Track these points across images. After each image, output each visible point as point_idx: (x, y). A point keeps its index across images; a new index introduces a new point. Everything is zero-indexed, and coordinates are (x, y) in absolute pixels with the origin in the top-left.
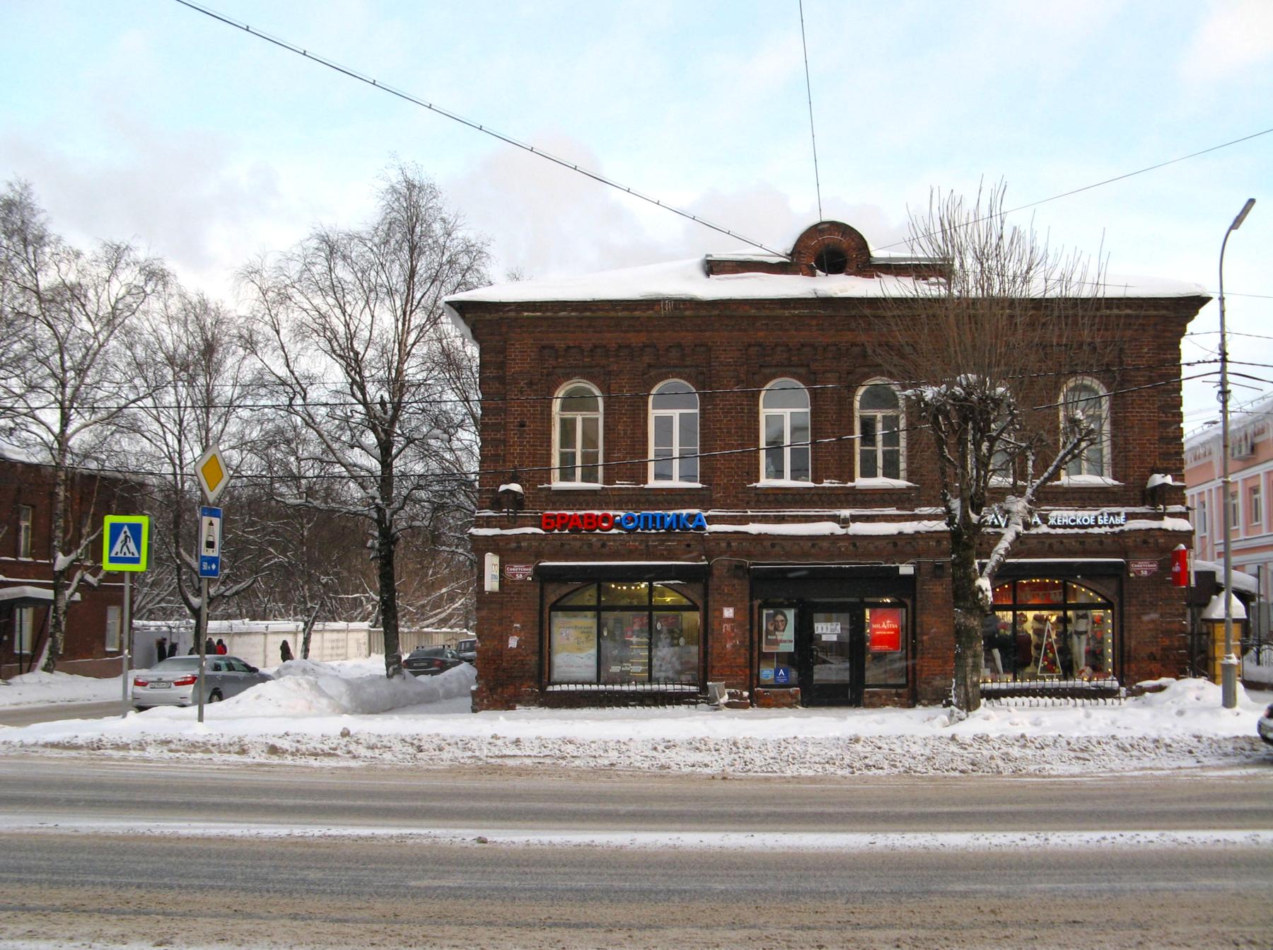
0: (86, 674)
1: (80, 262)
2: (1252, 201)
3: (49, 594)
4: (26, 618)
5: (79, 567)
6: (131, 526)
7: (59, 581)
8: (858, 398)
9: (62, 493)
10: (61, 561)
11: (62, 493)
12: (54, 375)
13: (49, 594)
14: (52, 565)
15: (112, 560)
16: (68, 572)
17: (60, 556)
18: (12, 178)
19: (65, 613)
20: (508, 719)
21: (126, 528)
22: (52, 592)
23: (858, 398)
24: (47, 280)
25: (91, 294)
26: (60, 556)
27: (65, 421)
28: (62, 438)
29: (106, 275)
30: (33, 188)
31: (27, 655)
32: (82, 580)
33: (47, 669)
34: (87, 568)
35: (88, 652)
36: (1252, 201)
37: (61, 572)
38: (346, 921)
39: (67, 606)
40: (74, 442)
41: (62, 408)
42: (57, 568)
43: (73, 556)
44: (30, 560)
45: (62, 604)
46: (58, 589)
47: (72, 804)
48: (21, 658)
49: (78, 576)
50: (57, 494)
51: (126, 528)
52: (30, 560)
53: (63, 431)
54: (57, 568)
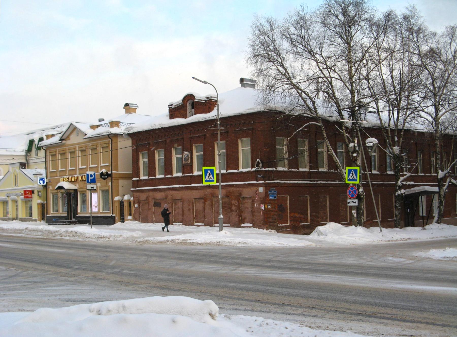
0: (448, 224)
1: (436, 38)
2: (193, 78)
3: (436, 189)
4: (423, 200)
5: (448, 176)
6: (210, 170)
7: (440, 183)
8: (314, 123)
9: (438, 143)
10: (441, 174)
11: (438, 143)
12: (431, 91)
13: (436, 189)
14: (437, 176)
15: (206, 181)
16: (444, 179)
17: (440, 172)
18: (407, 5)
19: (444, 197)
20: (96, 228)
21: (209, 171)
22: (437, 188)
23: (314, 123)
24: (425, 48)
25: (443, 51)
26: (440, 172)
27: (437, 110)
28: (436, 119)
29: (449, 41)
30: (417, 7)
31: (425, 216)
32: (450, 182)
33: (438, 222)
34: (452, 177)
35: (449, 215)
36: (193, 78)
37: (441, 179)
38: (103, 279)
39: (445, 194)
40: (442, 119)
41: (435, 105)
42: (439, 177)
43: (446, 172)
44: (423, 174)
45: (442, 193)
46: (440, 186)
47: (387, 276)
48: (423, 217)
49: (448, 180)
50: (437, 144)
51: (209, 171)
52: (423, 174)
53: (436, 115)
54: (439, 177)
